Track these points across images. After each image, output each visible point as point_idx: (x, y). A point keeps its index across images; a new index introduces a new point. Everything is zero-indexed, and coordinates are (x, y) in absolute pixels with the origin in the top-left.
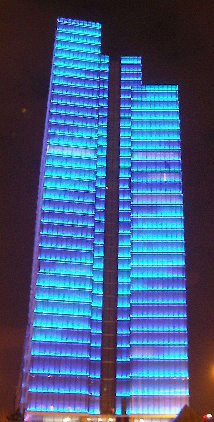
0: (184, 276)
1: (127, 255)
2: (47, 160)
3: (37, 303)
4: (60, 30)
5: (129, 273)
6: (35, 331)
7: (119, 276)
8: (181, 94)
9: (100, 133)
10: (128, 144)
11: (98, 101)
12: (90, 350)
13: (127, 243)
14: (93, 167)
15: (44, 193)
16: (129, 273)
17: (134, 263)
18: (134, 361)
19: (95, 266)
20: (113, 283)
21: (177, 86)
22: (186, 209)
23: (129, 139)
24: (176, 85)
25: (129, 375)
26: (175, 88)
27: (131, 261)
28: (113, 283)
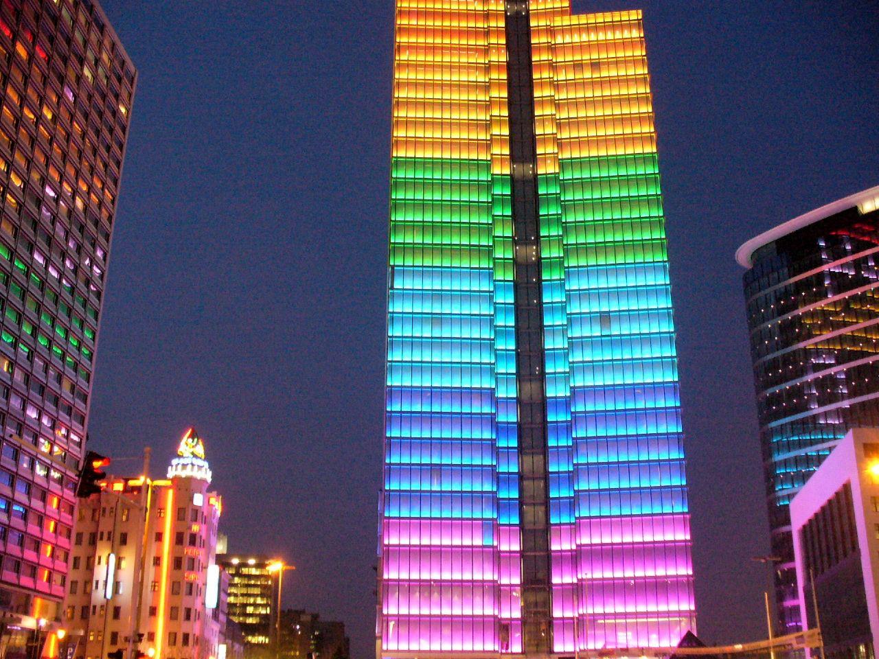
0: (686, 510)
1: (559, 297)
2: (387, 452)
3: (400, 48)
4: (402, 39)
5: (568, 428)
6: (397, 185)
7: (546, 361)
8: (645, 24)
9: (495, 131)
10: (554, 189)
11: (487, 87)
12: (497, 592)
13: (561, 367)
14: (485, 219)
15: (386, 508)
16: (568, 428)
17: (577, 356)
18: (585, 550)
19: (501, 369)
20: (542, 553)
21: (640, 11)
22: (679, 291)
23: (555, 158)
24: (637, 9)
25: (577, 575)
26: (635, 15)
27: (575, 481)
28: (542, 553)
